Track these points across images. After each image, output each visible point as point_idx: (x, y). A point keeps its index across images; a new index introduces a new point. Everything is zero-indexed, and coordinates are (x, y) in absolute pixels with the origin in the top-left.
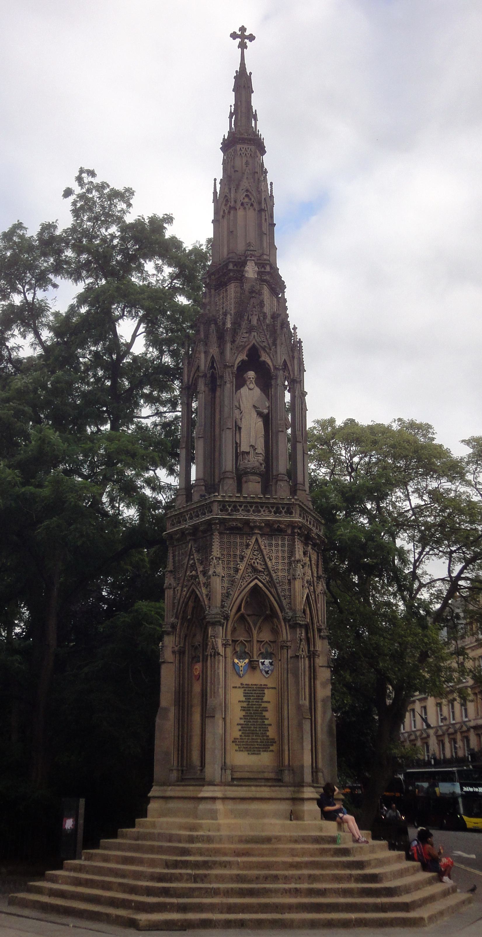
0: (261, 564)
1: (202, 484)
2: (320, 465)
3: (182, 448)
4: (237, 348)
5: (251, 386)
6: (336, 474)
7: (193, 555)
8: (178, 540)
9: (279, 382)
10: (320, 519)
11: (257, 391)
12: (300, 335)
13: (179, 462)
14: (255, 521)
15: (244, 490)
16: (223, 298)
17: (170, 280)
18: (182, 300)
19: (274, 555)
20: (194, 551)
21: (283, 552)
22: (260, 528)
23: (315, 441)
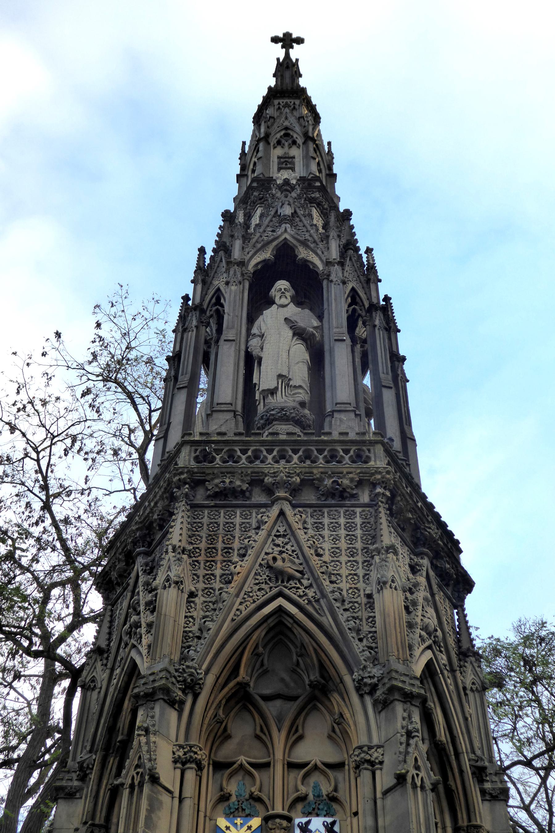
19: (327, 546)
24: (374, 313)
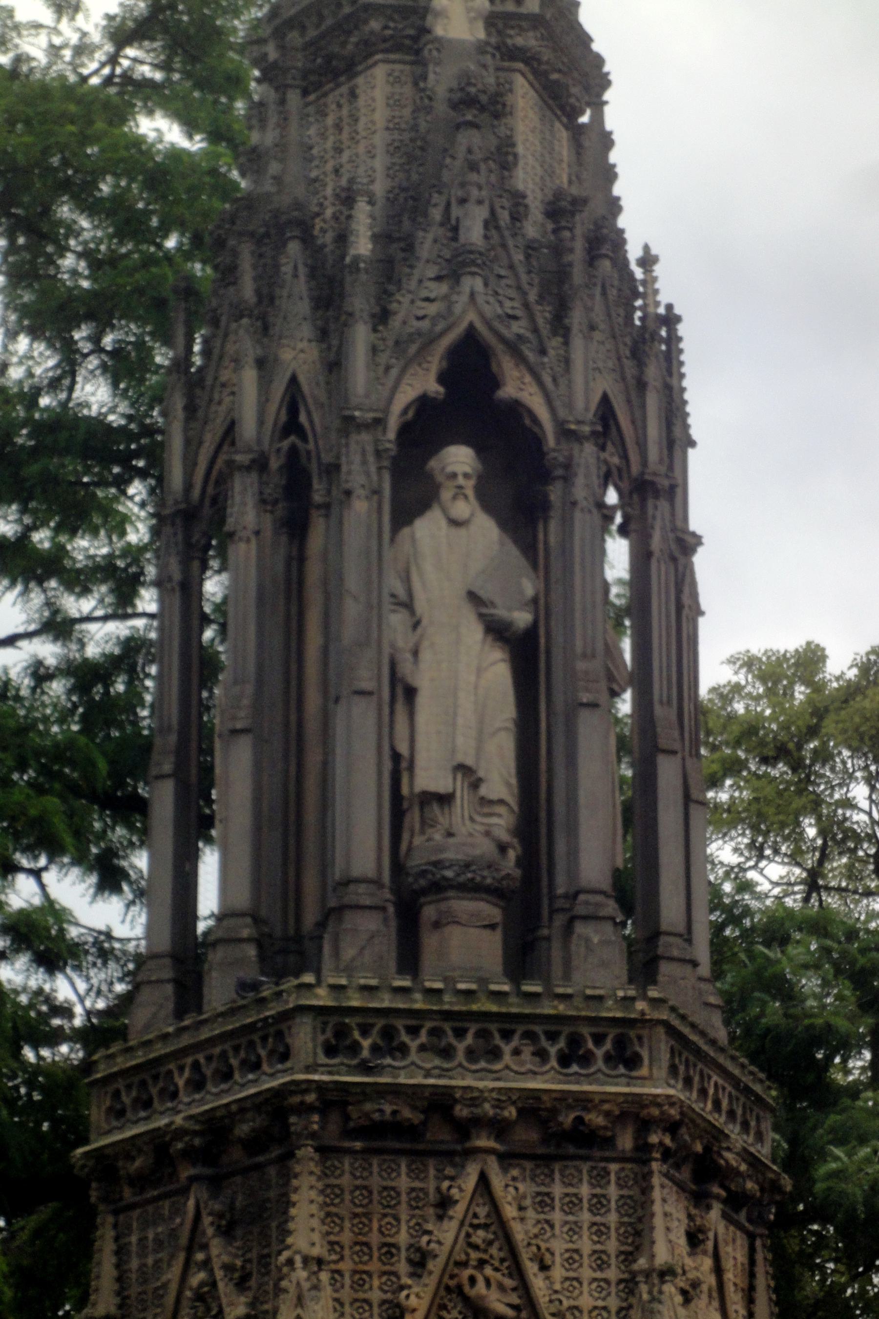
0: (501, 1288)
1: (245, 933)
2: (761, 849)
3: (161, 777)
4: (397, 343)
5: (462, 509)
6: (828, 889)
7: (205, 1247)
8: (140, 1182)
9: (580, 492)
10: (758, 1088)
11: (485, 531)
12: (671, 288)
13: (145, 837)
14: (475, 1099)
15: (428, 959)
16: (338, 127)
17: (109, 48)
18: (160, 130)
19: (559, 1246)
20: (210, 1231)
21: (599, 1233)
22: (499, 1128)
23: (737, 744)
24: (650, 503)
